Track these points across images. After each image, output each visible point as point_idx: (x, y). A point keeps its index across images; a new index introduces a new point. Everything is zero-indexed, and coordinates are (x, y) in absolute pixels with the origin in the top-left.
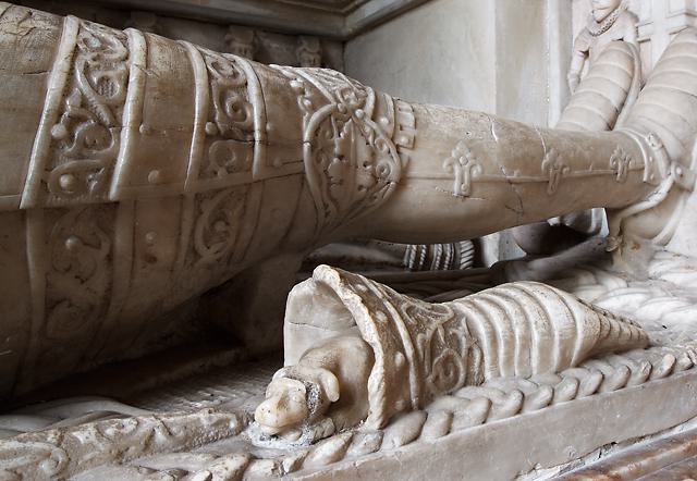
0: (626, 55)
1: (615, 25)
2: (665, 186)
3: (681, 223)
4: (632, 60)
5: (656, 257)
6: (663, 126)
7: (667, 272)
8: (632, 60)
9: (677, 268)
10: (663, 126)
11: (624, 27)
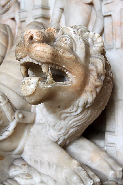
0: (4, 33)
1: (10, 10)
2: (12, 126)
3: (27, 144)
4: (7, 36)
5: (15, 163)
6: (9, 88)
7: (18, 176)
8: (7, 36)
9: (22, 174)
10: (9, 88)
11: (14, 11)
